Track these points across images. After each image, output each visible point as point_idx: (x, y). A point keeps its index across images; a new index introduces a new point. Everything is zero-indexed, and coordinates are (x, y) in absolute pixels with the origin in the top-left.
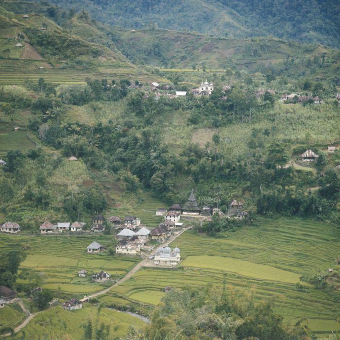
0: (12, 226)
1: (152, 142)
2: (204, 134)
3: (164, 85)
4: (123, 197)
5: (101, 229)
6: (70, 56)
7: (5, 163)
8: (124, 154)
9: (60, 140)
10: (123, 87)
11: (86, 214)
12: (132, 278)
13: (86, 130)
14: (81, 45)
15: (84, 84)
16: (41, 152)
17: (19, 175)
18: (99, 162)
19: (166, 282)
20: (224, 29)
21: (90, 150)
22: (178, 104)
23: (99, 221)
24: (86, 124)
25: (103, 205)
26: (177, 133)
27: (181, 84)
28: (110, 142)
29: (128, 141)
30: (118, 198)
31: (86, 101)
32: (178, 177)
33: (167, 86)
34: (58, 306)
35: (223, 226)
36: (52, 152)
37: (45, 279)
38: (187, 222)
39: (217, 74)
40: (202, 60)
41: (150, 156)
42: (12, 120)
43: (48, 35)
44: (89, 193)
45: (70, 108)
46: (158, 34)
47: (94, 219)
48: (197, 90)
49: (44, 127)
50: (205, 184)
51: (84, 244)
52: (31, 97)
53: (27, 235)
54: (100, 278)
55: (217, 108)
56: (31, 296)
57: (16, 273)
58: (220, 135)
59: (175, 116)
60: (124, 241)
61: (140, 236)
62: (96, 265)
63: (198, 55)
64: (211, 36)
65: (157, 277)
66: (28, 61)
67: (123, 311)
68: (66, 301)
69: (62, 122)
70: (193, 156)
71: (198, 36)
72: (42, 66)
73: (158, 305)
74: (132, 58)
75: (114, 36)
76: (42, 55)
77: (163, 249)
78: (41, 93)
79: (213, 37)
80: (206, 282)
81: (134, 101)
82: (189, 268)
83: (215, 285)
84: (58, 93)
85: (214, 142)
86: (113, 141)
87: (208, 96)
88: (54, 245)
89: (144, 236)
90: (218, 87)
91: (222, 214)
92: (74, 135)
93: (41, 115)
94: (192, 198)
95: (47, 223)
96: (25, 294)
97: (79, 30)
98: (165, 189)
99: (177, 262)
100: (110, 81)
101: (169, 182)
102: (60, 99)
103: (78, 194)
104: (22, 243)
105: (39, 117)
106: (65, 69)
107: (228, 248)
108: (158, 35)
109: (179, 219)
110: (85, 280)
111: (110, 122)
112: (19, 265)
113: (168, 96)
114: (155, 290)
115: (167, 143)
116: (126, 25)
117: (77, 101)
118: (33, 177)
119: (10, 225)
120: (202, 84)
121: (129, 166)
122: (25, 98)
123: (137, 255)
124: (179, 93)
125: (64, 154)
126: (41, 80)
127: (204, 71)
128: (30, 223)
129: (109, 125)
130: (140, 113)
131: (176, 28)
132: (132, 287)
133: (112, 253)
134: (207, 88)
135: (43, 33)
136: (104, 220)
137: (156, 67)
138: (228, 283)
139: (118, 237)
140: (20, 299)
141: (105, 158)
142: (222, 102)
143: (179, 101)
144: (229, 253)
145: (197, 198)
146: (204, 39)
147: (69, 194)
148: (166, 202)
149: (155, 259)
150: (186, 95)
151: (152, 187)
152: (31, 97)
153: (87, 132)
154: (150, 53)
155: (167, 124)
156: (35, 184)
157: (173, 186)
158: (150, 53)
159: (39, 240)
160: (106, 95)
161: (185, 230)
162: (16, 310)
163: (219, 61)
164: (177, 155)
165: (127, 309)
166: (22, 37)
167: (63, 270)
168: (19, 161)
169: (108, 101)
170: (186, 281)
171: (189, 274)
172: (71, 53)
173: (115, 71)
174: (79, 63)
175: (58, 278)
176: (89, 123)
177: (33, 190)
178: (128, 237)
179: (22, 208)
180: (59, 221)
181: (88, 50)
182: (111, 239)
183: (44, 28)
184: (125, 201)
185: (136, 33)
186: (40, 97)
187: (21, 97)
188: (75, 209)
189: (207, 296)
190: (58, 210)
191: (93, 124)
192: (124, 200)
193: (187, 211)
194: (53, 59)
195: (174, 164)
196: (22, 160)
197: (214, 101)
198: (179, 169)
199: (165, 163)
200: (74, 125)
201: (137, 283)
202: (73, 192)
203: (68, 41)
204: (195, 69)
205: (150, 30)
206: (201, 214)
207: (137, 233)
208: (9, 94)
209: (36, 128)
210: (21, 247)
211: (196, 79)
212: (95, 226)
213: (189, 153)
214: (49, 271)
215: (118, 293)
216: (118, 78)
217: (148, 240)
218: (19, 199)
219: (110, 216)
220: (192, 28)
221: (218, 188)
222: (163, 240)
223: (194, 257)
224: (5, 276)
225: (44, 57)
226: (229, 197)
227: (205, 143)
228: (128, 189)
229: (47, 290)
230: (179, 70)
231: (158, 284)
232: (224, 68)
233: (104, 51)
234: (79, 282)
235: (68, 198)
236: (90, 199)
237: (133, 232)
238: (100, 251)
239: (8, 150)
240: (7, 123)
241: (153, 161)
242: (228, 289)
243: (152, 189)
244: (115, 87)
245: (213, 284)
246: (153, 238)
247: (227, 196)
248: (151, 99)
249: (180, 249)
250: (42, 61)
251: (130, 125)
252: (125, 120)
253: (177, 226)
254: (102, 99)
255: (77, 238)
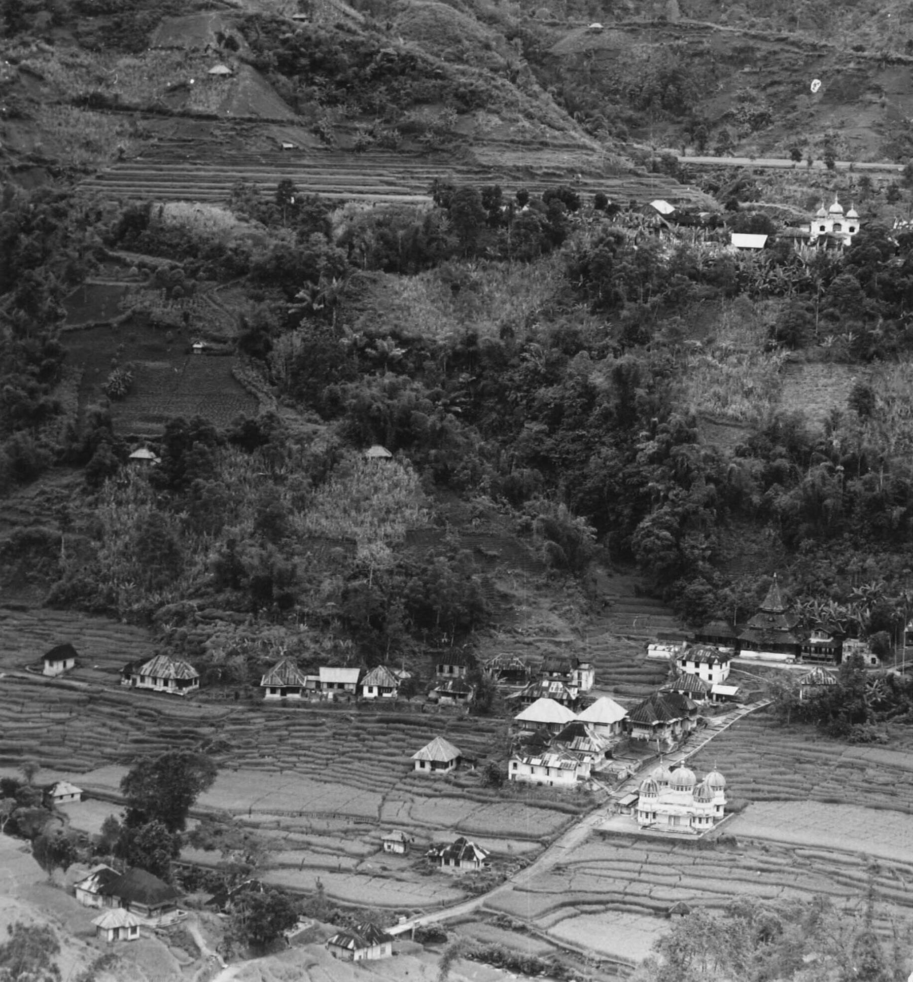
0: (172, 671)
1: (641, 404)
2: (823, 381)
3: (692, 210)
4: (538, 588)
5: (462, 696)
6: (383, 108)
7: (159, 460)
8: (549, 442)
9: (338, 388)
10: (553, 214)
11: (413, 642)
12: (559, 869)
13: (426, 357)
14: (421, 71)
15: (424, 202)
16: (273, 428)
17: (198, 502)
18: (464, 468)
19: (675, 886)
20: (903, 28)
21: (434, 425)
22: (738, 276)
23: (456, 669)
24: (424, 336)
25: (472, 612)
26: (729, 376)
27: (750, 209)
28: (502, 400)
29: (562, 398)
30: (522, 593)
31: (427, 259)
32: (727, 529)
33: (702, 214)
34: (312, 945)
35: (875, 703)
36: (311, 427)
37: (273, 853)
38: (756, 685)
39: (875, 178)
40: (823, 129)
41: (636, 452)
42: (186, 317)
43: (314, 36)
44: (425, 570)
45: (374, 281)
46: (677, 38)
47: (440, 660)
48: (804, 230)
49: (291, 343)
50: (820, 554)
51: (404, 744)
52: (250, 242)
53: (219, 702)
54: (452, 863)
55: (869, 296)
56: (228, 905)
57: (183, 829)
58: (877, 387)
59: (725, 317)
60: (540, 739)
61: (591, 727)
62: (442, 815)
63: (812, 110)
64: (859, 49)
65: (647, 867)
66: (248, 125)
67: (527, 974)
68: (342, 929)
69: (346, 327)
70: (782, 457)
71: (814, 47)
72: (291, 138)
73: (646, 963)
74: (587, 116)
75: (531, 45)
76: (293, 102)
77: (668, 775)
78: (283, 231)
79: (866, 53)
80: (810, 891)
81: (588, 264)
82: (756, 844)
83: (840, 903)
84: (339, 232)
85: (855, 412)
86: (512, 396)
87: (839, 254)
88: (307, 743)
89: (605, 725)
90: (875, 223)
91: (873, 660)
92: (383, 375)
93: (281, 303)
94: (774, 601)
95: (285, 667)
96: (210, 897)
97: (416, 20)
98: (684, 568)
99: (715, 820)
100: (509, 194)
101: (697, 544)
102: (340, 252)
103: (390, 572)
104: (205, 730)
105: (272, 311)
106: (364, 151)
107: (888, 778)
108: (680, 42)
109: (726, 674)
110: (404, 863)
111: (506, 331)
112: (190, 802)
113: (704, 248)
114: (637, 912)
115: (693, 410)
116: (570, 8)
117: (399, 260)
118: (244, 510)
119: (167, 667)
120: (821, 211)
121: (562, 483)
122: (232, 245)
123: (579, 789)
124: (740, 240)
125: (349, 436)
126: (286, 187)
127: (830, 165)
128: (230, 663)
129: (502, 343)
130: (608, 305)
131: (741, 19)
132: (550, 902)
133: (496, 779)
134: (837, 226)
135: (299, 30)
136: (472, 663)
137: (667, 150)
138: (885, 897)
139: (517, 725)
140: (193, 913)
141: (482, 452)
142: (885, 275)
143: (742, 265)
144: (893, 794)
145: (790, 601)
146: (834, 60)
147: (362, 571)
148: (682, 614)
149: (640, 806)
150: (766, 245)
151: (638, 557)
152: (250, 242)
153: (428, 364)
154: (648, 102)
155: (699, 344)
156: (252, 535)
157: (710, 560)
158: (648, 102)
159: (259, 721)
160: (495, 239)
161: (744, 713)
162: (178, 951)
163: (881, 133)
164: (729, 452)
165: (542, 968)
166: (231, 44)
167: (331, 828)
168: (202, 454)
169: (500, 260)
170: (742, 888)
171: (753, 863)
172: (385, 98)
173: (527, 159)
174: (410, 130)
175: (314, 851)
176: (435, 334)
177: (242, 553)
178: (551, 726)
179: (207, 611)
180: (325, 663)
181: (444, 87)
182: (492, 731)
183: (303, 16)
184: (546, 603)
185: (605, 35)
186: (281, 243)
187: (217, 241)
188: (378, 622)
189: (811, 940)
190: (321, 623)
191: (449, 338)
192: (542, 600)
193: (753, 647)
194: (327, 118)
195: (717, 482)
196: (213, 453)
197: (860, 270)
198: (731, 502)
199: (684, 479)
200: (384, 337)
201: (575, 886)
202: (373, 565)
203: (378, 58)
204: (799, 160)
205: (653, 24)
206: (801, 659)
207: (583, 716)
208: (181, 230)
209: (260, 346)
210: (201, 742)
211: (798, 191)
212: (443, 683)
213: (769, 444)
214: (287, 828)
215: (513, 914)
216: (537, 183)
217: (618, 740)
218: (199, 581)
219: (494, 653)
220: (793, 20)
221: (864, 571)
222: (670, 741)
223: (774, 805)
224: (144, 836)
225: (298, 112)
226: (899, 604)
227: (824, 413)
228: (558, 562)
229: (280, 889)
230: (745, 161)
231: (647, 892)
232: (898, 159)
233: (495, 92)
234: (384, 869)
235: (356, 583)
236: (428, 590)
237: (570, 712)
238: (456, 769)
239: (167, 419)
240: (169, 327)
241: (645, 470)
242: (883, 917)
243: (638, 567)
244: (525, 214)
245: (833, 900)
246: (636, 733)
247: (893, 601)
248: (645, 258)
249: (727, 776)
250: (292, 123)
251: (569, 344)
252: (557, 326)
253: (719, 696)
254: (483, 254)
255: (380, 721)
